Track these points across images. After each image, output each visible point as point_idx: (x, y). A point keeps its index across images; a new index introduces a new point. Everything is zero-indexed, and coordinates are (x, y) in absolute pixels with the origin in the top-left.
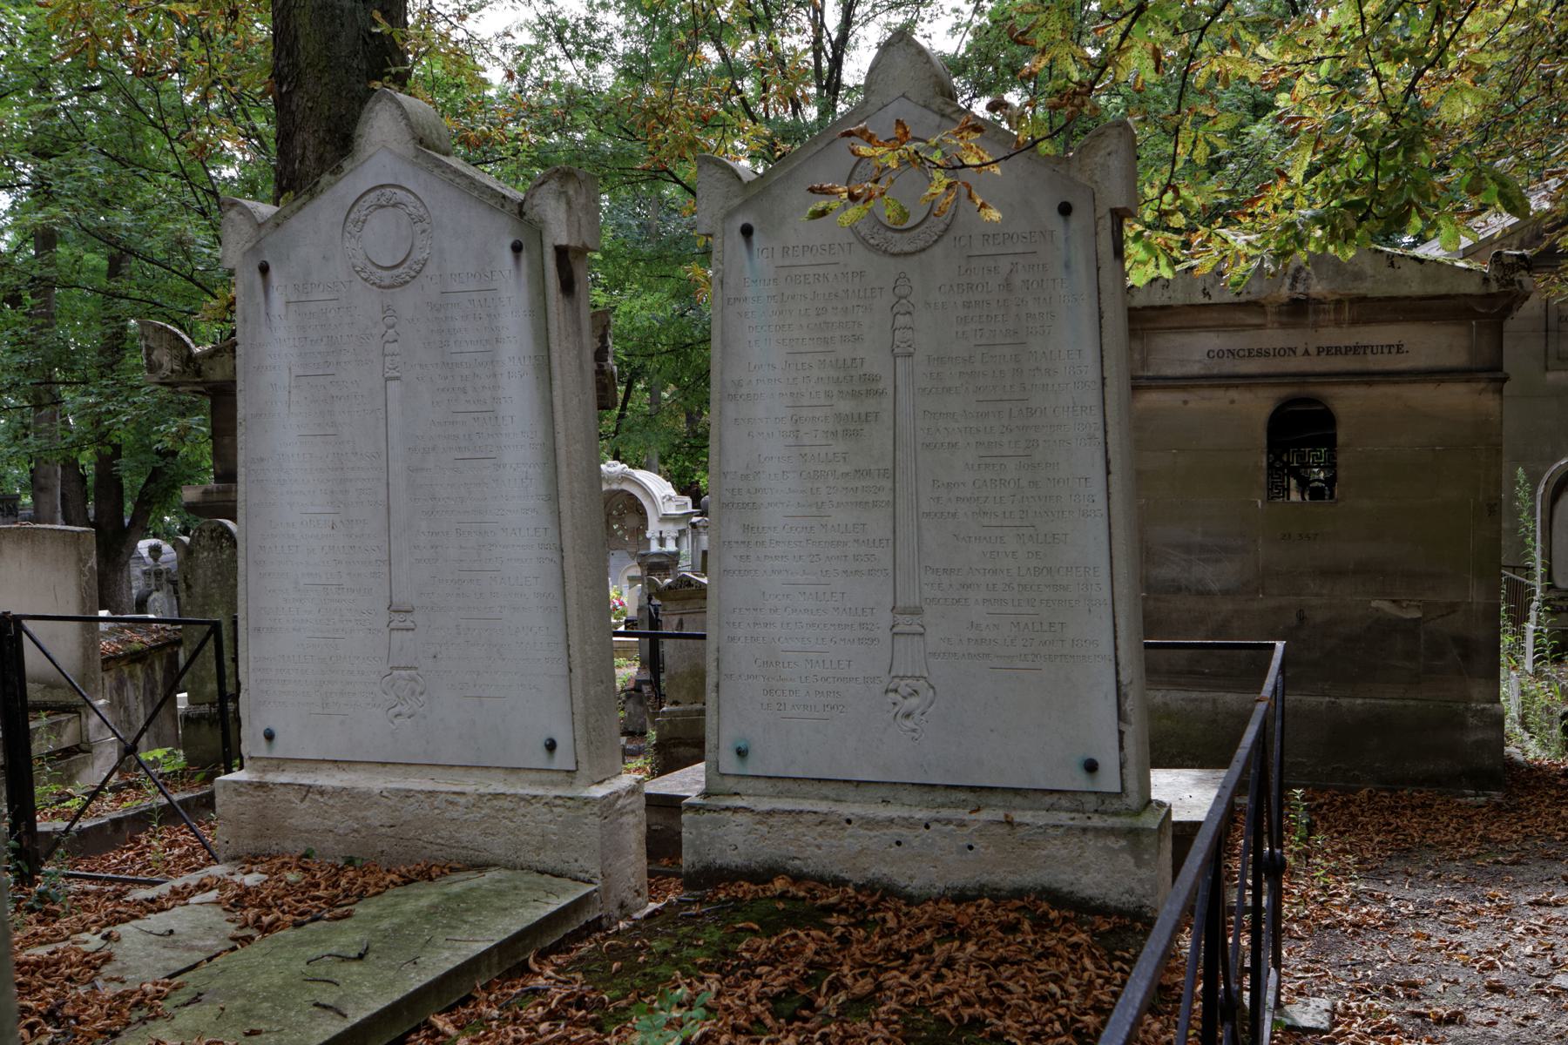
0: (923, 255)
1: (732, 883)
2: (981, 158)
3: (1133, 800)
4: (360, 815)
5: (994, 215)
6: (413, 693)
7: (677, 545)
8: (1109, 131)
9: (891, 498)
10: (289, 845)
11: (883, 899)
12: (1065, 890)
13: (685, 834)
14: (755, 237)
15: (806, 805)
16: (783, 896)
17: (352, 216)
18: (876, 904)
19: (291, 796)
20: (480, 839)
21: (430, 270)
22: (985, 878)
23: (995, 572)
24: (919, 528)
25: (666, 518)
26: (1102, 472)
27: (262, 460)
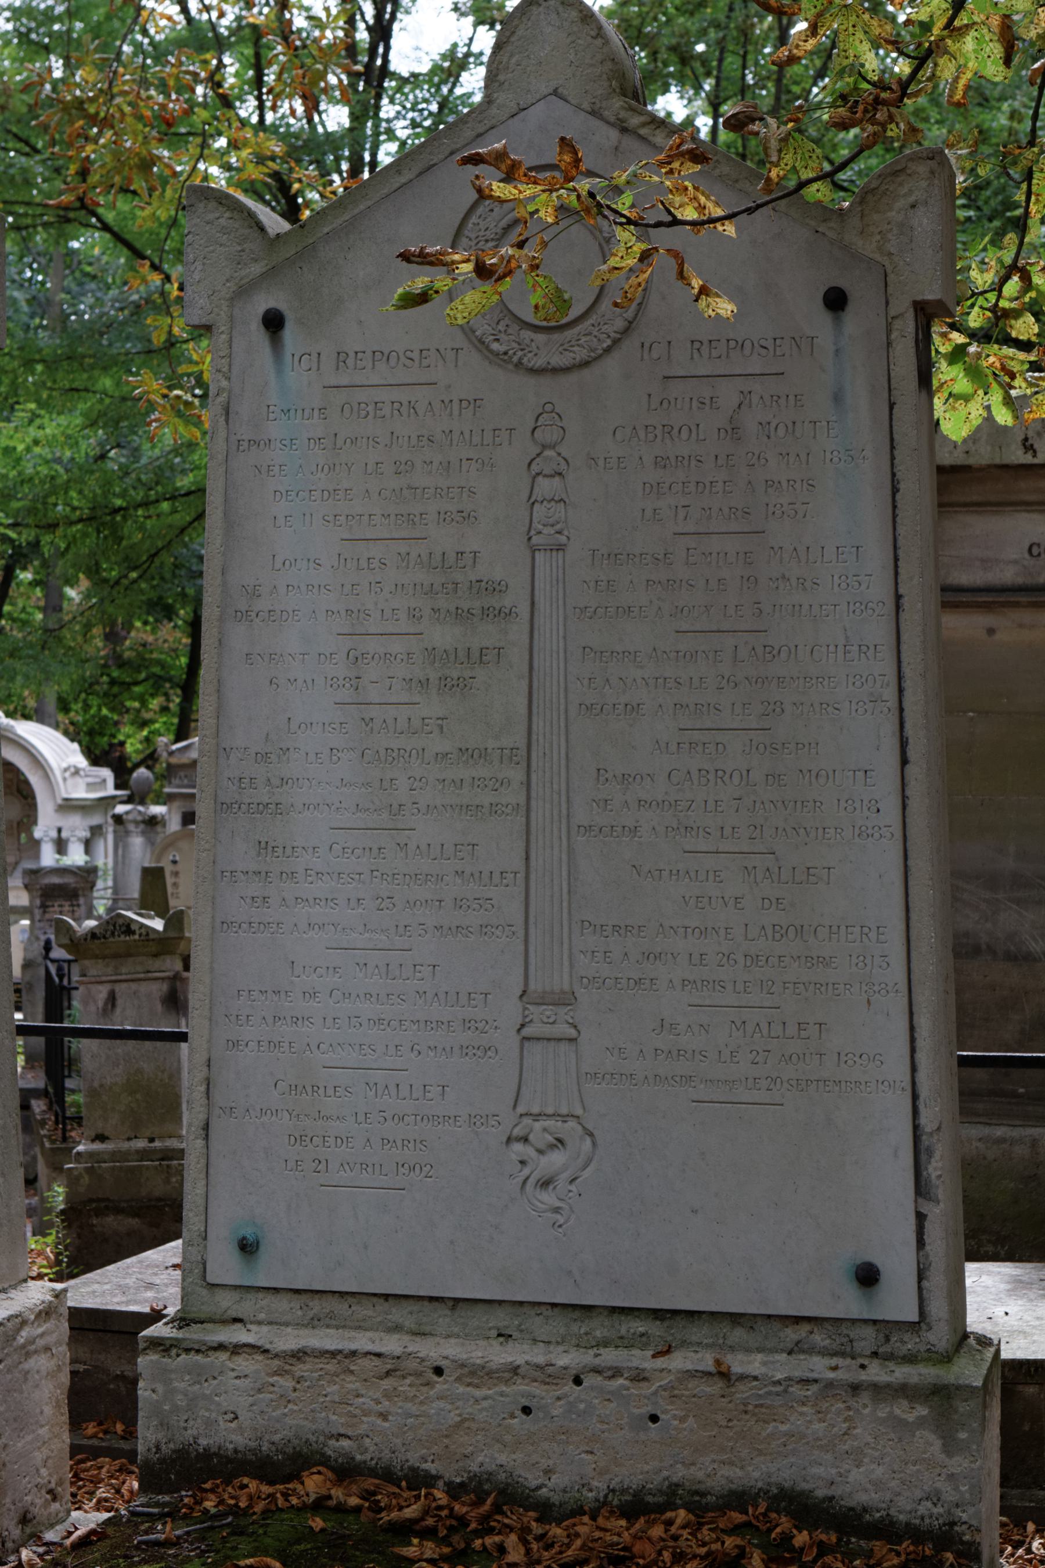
0: (586, 372)
1: (228, 1482)
2: (701, 208)
3: (939, 1337)
5: (725, 307)
7: (87, 851)
8: (913, 167)
9: (522, 800)
11: (497, 1509)
12: (820, 1493)
13: (143, 1391)
14: (289, 333)
15: (362, 1342)
16: (320, 1505)
18: (485, 1519)
22: (679, 1474)
23: (704, 932)
24: (570, 851)
25: (68, 806)
26: (895, 760)
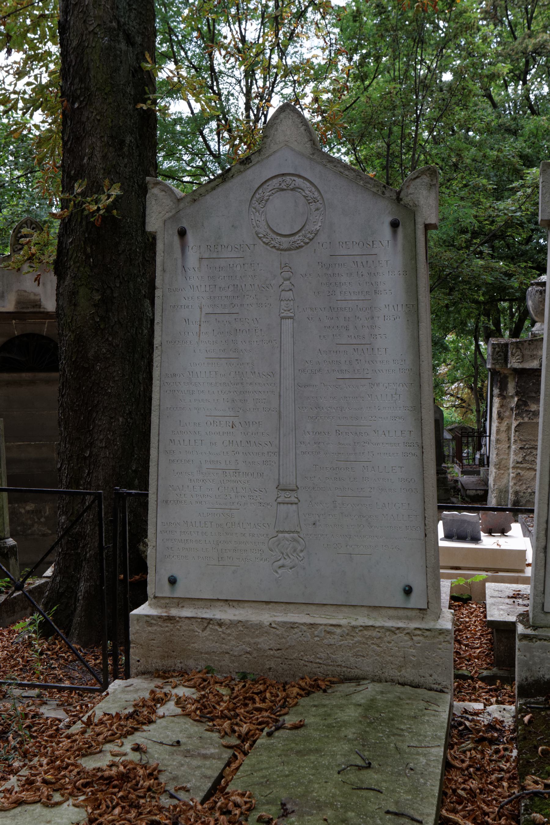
4: (252, 641)
6: (295, 551)
10: (191, 663)
17: (257, 196)
19: (195, 627)
20: (352, 660)
21: (322, 238)
27: (175, 375)
